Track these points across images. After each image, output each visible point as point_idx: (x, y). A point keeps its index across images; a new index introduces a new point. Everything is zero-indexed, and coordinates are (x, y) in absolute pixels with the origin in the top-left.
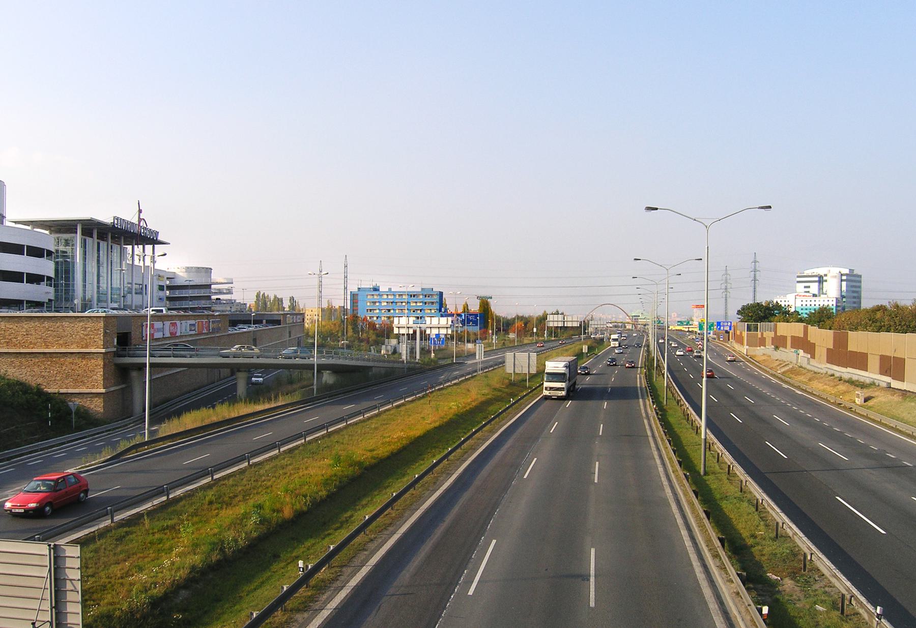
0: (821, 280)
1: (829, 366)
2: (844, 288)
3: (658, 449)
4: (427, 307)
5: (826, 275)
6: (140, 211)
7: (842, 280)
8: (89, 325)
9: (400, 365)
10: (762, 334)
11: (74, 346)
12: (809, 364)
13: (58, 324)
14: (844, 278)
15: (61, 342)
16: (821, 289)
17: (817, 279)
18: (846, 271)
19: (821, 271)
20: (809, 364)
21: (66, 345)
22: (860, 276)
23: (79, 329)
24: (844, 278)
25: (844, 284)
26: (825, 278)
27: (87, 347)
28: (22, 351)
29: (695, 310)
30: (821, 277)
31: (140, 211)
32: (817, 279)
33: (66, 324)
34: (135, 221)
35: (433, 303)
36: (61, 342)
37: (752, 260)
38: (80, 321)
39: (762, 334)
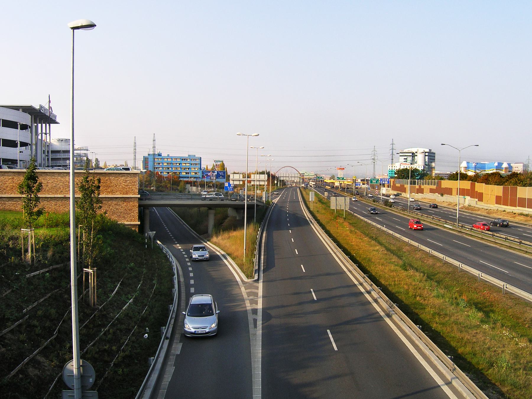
0: (413, 155)
1: (497, 205)
2: (427, 160)
3: (335, 253)
4: (192, 166)
5: (416, 152)
6: (50, 102)
7: (425, 156)
8: (129, 179)
9: (262, 204)
10: (420, 187)
11: (118, 193)
12: (477, 204)
13: (107, 178)
14: (427, 154)
15: (109, 190)
16: (413, 160)
17: (411, 154)
18: (428, 151)
19: (414, 150)
20: (477, 204)
21: (112, 192)
22: (435, 153)
23: (121, 182)
24: (427, 154)
25: (427, 157)
26: (416, 154)
27: (127, 194)
28: (56, 196)
29: (339, 171)
30: (413, 153)
31: (50, 102)
32: (411, 154)
33: (112, 178)
34: (47, 107)
35: (196, 164)
36: (109, 190)
37: (391, 143)
38: (122, 176)
39: (420, 187)
